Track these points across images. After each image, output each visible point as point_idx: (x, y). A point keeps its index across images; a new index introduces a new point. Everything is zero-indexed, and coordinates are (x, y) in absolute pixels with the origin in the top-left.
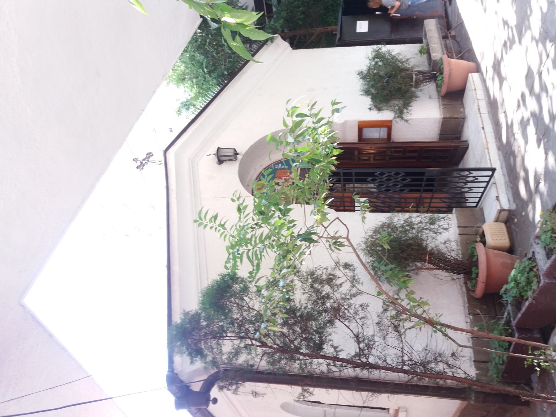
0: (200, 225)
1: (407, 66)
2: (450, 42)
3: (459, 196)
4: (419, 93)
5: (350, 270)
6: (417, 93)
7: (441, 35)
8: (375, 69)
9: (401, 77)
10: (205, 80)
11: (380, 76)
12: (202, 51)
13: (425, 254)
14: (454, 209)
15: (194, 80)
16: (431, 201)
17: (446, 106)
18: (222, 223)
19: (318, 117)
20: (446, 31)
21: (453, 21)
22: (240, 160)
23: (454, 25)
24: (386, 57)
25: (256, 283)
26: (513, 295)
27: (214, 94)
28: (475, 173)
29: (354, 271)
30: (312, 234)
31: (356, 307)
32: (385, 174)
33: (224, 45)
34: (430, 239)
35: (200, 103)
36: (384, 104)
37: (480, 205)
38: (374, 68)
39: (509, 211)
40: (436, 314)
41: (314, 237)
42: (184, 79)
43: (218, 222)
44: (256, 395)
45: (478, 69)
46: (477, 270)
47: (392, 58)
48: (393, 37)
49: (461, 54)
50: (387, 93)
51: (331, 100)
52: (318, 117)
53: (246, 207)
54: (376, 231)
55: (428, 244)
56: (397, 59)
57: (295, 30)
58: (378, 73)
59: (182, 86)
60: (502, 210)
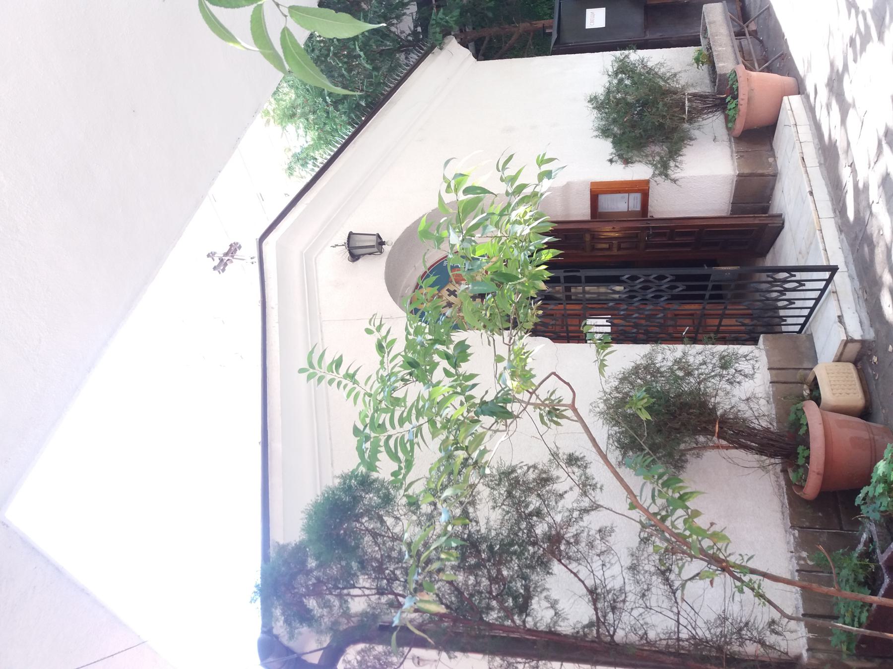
0: (309, 378)
1: (674, 85)
2: (747, 42)
3: (770, 314)
4: (695, 133)
5: (579, 467)
6: (692, 132)
7: (732, 30)
8: (619, 92)
9: (665, 105)
10: (328, 117)
11: (627, 104)
12: (323, 67)
13: (713, 423)
14: (762, 336)
15: (311, 117)
16: (720, 322)
17: (742, 154)
18: (351, 371)
19: (517, 183)
20: (742, 24)
21: (752, 6)
22: (388, 253)
23: (754, 13)
24: (638, 71)
25: (406, 490)
26: (882, 509)
27: (344, 141)
28: (799, 276)
29: (586, 467)
30: (506, 401)
31: (590, 533)
32: (640, 278)
33: (360, 56)
34: (721, 393)
35: (324, 156)
36: (635, 152)
37: (807, 329)
38: (617, 89)
39: (863, 342)
40: (740, 555)
41: (511, 407)
42: (293, 115)
43: (343, 370)
44: (419, 663)
45: (799, 88)
46: (807, 451)
47: (647, 72)
48: (648, 36)
49: (769, 62)
50: (640, 133)
52: (517, 183)
53: (393, 341)
54: (624, 379)
55: (719, 403)
56: (656, 73)
57: (483, 27)
58: (623, 98)
59: (291, 127)
60: (849, 341)
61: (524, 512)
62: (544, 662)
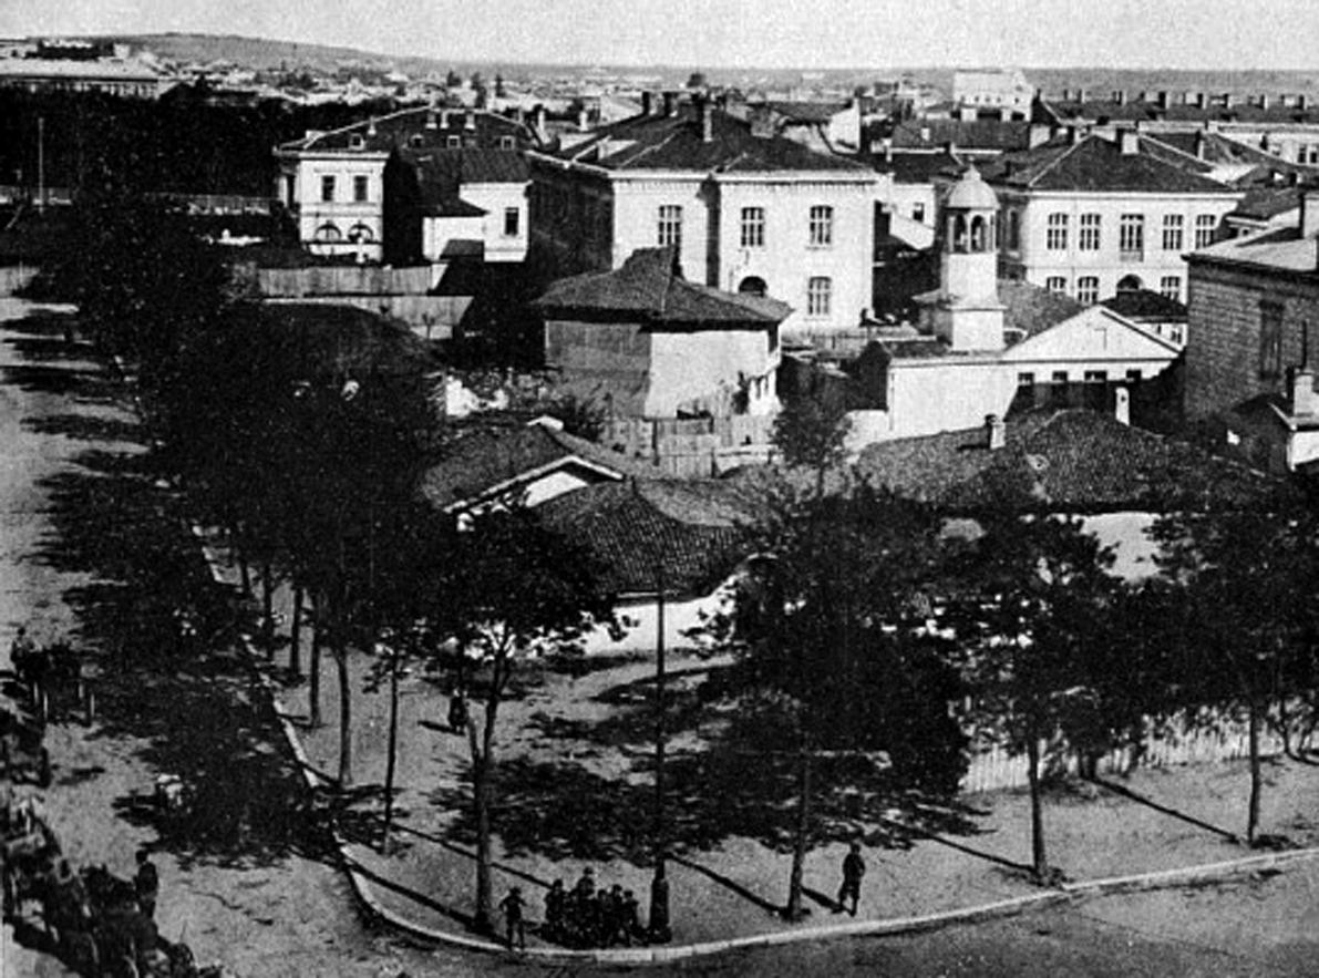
18: (763, 383)
51: (859, 311)
61: (1133, 131)
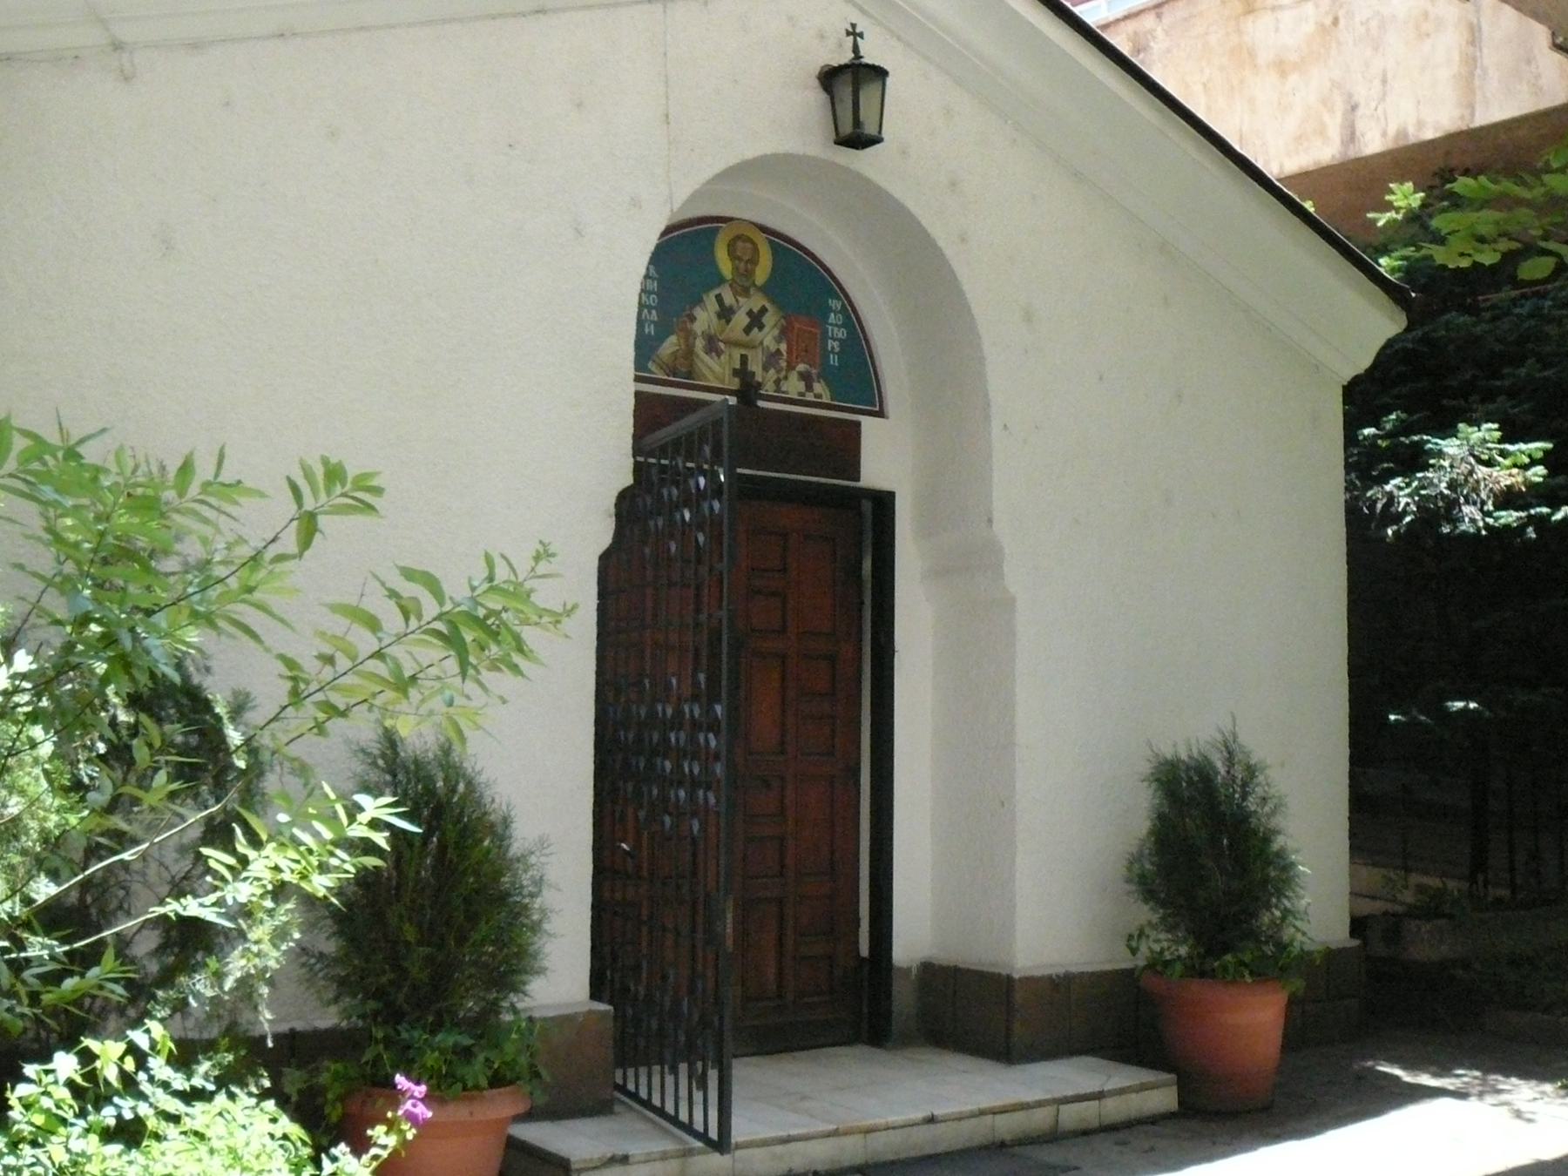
37: (623, 1103)
62: (348, 1150)
